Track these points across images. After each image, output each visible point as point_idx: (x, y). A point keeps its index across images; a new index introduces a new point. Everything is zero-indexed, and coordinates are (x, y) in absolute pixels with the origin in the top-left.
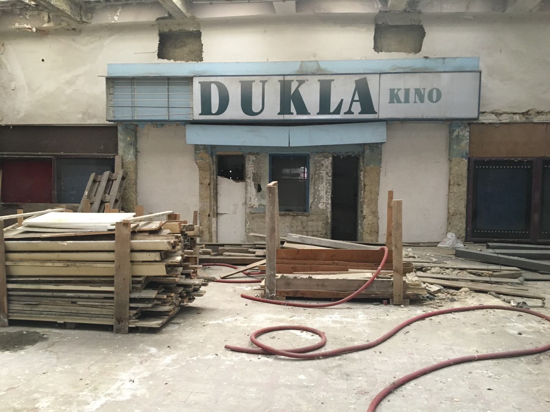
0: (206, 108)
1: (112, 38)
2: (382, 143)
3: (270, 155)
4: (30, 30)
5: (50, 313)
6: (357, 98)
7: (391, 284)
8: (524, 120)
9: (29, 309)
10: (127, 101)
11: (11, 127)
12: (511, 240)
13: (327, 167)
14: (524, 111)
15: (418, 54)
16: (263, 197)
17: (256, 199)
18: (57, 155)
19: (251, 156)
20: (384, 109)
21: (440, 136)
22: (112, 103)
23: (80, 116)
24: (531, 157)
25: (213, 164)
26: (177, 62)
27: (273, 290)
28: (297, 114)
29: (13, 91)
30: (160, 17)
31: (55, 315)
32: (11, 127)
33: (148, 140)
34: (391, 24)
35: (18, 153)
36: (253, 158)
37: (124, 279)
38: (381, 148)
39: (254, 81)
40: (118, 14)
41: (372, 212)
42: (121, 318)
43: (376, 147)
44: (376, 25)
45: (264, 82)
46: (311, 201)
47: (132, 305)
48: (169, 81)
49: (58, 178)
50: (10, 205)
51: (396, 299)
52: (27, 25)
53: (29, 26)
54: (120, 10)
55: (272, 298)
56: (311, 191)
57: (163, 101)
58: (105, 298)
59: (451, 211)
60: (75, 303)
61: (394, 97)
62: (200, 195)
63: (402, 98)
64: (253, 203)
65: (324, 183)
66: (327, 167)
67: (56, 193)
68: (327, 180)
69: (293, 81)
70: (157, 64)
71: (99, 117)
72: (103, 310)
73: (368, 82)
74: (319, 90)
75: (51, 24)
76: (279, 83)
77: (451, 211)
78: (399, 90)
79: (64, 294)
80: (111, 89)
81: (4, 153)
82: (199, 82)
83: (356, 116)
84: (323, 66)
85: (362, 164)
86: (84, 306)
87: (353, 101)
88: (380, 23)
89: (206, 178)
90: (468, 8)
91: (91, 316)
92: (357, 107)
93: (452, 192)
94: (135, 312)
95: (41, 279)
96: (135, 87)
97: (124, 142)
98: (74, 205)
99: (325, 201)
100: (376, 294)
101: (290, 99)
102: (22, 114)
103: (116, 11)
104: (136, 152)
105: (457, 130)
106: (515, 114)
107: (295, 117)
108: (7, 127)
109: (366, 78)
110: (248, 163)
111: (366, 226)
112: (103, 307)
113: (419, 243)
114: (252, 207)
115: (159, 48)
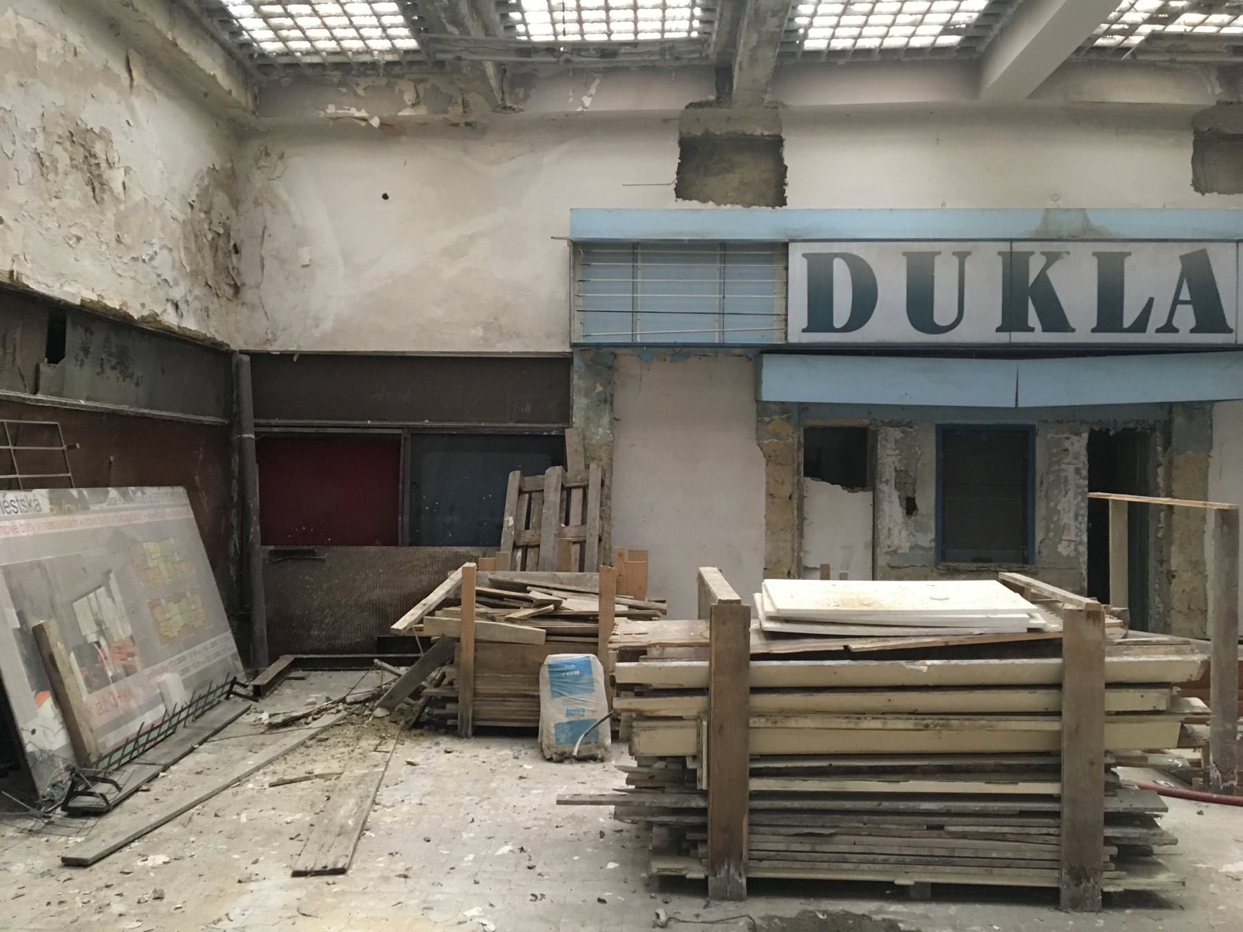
0: (820, 314)
2: (1212, 402)
3: (938, 427)
4: (363, 124)
5: (869, 857)
6: (1185, 295)
9: (808, 848)
10: (621, 298)
11: (295, 359)
13: (1077, 456)
16: (921, 528)
17: (904, 533)
18: (415, 428)
22: (580, 302)
23: (479, 332)
25: (799, 450)
26: (723, 207)
28: (1044, 330)
29: (306, 269)
30: (697, 99)
31: (885, 862)
32: (295, 359)
33: (641, 390)
34: (1227, 131)
35: (348, 423)
36: (895, 433)
39: (939, 253)
40: (593, 91)
41: (1190, 562)
43: (1199, 411)
45: (962, 257)
46: (1039, 536)
47: (1110, 832)
49: (413, 483)
50: (291, 553)
52: (359, 110)
53: (363, 114)
54: (597, 82)
55: (1229, 791)
56: (1041, 512)
57: (710, 299)
58: (1023, 814)
60: (941, 827)
64: (896, 543)
65: (1071, 494)
66: (1077, 456)
67: (406, 519)
68: (1078, 486)
69: (1032, 253)
71: (535, 329)
72: (1023, 846)
73: (1212, 262)
74: (1095, 275)
75: (422, 111)
76: (1000, 259)
79: (912, 805)
81: (273, 422)
82: (804, 255)
83: (1185, 336)
84: (1096, 221)
85: (1159, 449)
86: (964, 836)
87: (1176, 301)
89: (783, 483)
91: (990, 864)
92: (1186, 317)
94: (1114, 850)
95: (835, 763)
97: (586, 395)
99: (1072, 537)
101: (1025, 294)
102: (327, 326)
103: (587, 86)
104: (615, 420)
107: (1039, 336)
108: (286, 357)
109: (1204, 251)
110: (885, 447)
114: (895, 552)
115: (678, 173)
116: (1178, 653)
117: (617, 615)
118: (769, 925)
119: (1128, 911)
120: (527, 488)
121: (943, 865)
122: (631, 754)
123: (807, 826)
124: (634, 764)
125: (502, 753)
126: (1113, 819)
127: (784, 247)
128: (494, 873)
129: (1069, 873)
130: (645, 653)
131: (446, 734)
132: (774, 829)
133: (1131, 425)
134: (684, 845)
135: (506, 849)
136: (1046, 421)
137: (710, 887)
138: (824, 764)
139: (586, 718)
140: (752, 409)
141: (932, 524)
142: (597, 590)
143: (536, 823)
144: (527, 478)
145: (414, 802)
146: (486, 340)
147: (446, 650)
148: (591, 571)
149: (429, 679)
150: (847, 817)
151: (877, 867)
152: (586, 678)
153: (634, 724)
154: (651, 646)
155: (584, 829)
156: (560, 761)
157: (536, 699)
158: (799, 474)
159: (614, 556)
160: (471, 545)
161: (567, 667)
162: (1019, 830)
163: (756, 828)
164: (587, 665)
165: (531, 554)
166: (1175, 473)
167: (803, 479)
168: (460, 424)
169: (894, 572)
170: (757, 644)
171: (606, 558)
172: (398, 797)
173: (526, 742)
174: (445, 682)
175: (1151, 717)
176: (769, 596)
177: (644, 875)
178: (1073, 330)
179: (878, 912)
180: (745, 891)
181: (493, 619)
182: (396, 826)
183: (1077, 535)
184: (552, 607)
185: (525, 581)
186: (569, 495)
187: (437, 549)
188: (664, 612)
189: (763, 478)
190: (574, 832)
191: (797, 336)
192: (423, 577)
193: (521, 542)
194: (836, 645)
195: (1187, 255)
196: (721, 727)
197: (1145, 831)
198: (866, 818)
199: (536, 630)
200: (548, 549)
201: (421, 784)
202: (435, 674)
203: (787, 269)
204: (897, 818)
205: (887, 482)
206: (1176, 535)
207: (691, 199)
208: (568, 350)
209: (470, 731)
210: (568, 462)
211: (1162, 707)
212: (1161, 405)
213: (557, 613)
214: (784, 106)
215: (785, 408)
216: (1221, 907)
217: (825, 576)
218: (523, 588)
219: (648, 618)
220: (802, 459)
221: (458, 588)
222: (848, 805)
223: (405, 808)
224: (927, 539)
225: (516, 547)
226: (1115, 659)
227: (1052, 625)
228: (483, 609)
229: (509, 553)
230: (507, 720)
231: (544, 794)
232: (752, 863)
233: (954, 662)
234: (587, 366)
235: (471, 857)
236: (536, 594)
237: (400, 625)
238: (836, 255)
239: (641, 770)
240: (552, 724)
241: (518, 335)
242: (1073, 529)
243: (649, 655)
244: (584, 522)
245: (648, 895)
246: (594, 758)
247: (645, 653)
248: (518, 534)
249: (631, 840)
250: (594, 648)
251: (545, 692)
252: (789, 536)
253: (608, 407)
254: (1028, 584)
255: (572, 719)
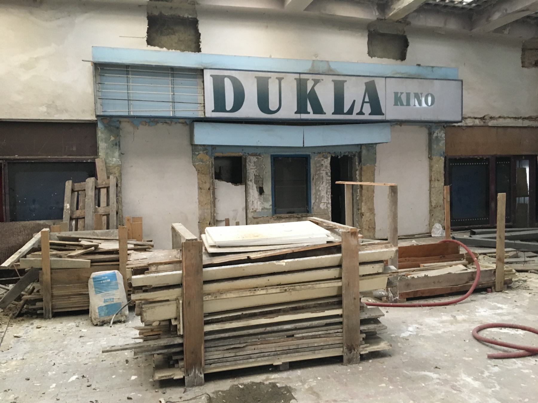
0: (220, 105)
1: (87, 15)
2: (376, 144)
3: (271, 156)
5: (262, 354)
6: (367, 99)
7: (493, 272)
8: (482, 124)
9: (233, 355)
10: (122, 93)
12: (478, 226)
13: (326, 167)
14: (482, 116)
15: (403, 62)
16: (266, 200)
17: (259, 203)
19: (252, 157)
20: (391, 111)
21: (421, 136)
22: (100, 94)
23: (44, 109)
24: (488, 155)
26: (170, 50)
27: (396, 293)
28: (314, 113)
31: (269, 356)
33: (133, 137)
36: (254, 159)
37: (355, 299)
38: (375, 148)
39: (270, 78)
42: (352, 345)
43: (371, 147)
44: (369, 31)
45: (280, 80)
46: (313, 201)
47: (363, 328)
48: (172, 72)
51: (498, 287)
56: (313, 191)
57: (168, 95)
58: (327, 325)
59: (433, 205)
60: (293, 336)
61: (398, 101)
62: (199, 202)
63: (405, 103)
64: (256, 207)
65: (324, 183)
66: (326, 167)
67: (8, 208)
69: (308, 79)
70: (145, 50)
72: (328, 339)
73: (376, 86)
77: (433, 205)
78: (402, 93)
80: (98, 77)
82: (211, 76)
84: (333, 67)
85: (357, 163)
86: (303, 338)
87: (364, 102)
88: (372, 30)
89: (205, 183)
90: (445, 24)
91: (314, 349)
92: (367, 109)
93: (434, 187)
95: (244, 313)
96: (130, 76)
97: (106, 142)
98: (38, 222)
99: (325, 201)
100: (482, 284)
101: (306, 98)
105: (436, 132)
106: (475, 118)
107: (311, 116)
109: (374, 81)
110: (250, 165)
111: (364, 223)
112: (327, 335)
113: (414, 235)
114: (255, 211)
115: (148, 33)
116: (387, 247)
117: (129, 250)
118: (217, 396)
119: (370, 361)
120: (76, 189)
121: (294, 353)
122: (142, 321)
123: (232, 344)
124: (142, 325)
125: (70, 325)
126: (364, 322)
127: (202, 70)
128: (68, 393)
129: (347, 348)
130: (148, 269)
131: (37, 318)
132: (216, 348)
133: (346, 154)
134: (171, 362)
135: (74, 378)
136: (314, 153)
137: (186, 381)
138: (239, 313)
139: (115, 302)
140: (190, 148)
141: (270, 198)
142: (117, 238)
143: (91, 360)
144: (76, 184)
145: (18, 358)
146: (48, 113)
147: (34, 274)
148: (113, 228)
149: (26, 290)
150: (251, 337)
151: (265, 358)
152: (114, 282)
153: (143, 306)
154: (150, 265)
155: (117, 359)
156: (102, 325)
157: (87, 295)
158: (213, 178)
159: (125, 221)
160: (46, 219)
161: (103, 278)
162: (325, 332)
163: (208, 349)
164: (114, 276)
165: (80, 222)
166: (363, 173)
167: (215, 180)
168: (37, 157)
169: (256, 220)
170: (206, 260)
171: (120, 222)
172: (9, 356)
173: (84, 317)
174: (35, 291)
175: (376, 276)
176: (209, 235)
177: (151, 380)
178: (325, 113)
179: (267, 379)
180: (203, 381)
181: (60, 257)
182: (8, 374)
183: (327, 200)
184: (93, 248)
185: (77, 236)
186: (99, 192)
187: (27, 222)
188: (153, 246)
189: (196, 181)
190: (111, 362)
191: (210, 114)
192: (20, 237)
193: (74, 216)
194: (244, 257)
195: (367, 83)
196: (189, 303)
197: (376, 325)
198: (259, 336)
199: (86, 261)
200: (89, 219)
201: (24, 347)
202: (30, 287)
203: (203, 82)
204: (273, 334)
205: (251, 181)
206: (364, 198)
207: (154, 46)
208: (94, 118)
209: (51, 315)
210: (98, 175)
211: (381, 271)
212: (357, 145)
213: (96, 251)
214: (198, 4)
215: (205, 147)
216: (405, 353)
217: (227, 224)
218: (77, 239)
219: (145, 250)
220: (214, 172)
221: (39, 241)
222: (251, 331)
223: (14, 363)
224: (269, 205)
225: (71, 219)
226: (362, 252)
227: (335, 239)
228: (55, 252)
229: (68, 222)
230: (71, 308)
231: (94, 344)
232: (206, 366)
233: (296, 259)
234: (105, 127)
235: (54, 385)
236: (84, 242)
237: (6, 264)
238: (226, 76)
239: (147, 327)
240: (97, 307)
241: (67, 111)
242: (326, 198)
243: (150, 271)
244: (108, 205)
245: (154, 391)
246: (120, 322)
247: (148, 269)
248: (72, 212)
249: (143, 362)
250: (117, 267)
251: (92, 291)
252: (209, 207)
253: (117, 147)
254: (322, 222)
255: (107, 304)
